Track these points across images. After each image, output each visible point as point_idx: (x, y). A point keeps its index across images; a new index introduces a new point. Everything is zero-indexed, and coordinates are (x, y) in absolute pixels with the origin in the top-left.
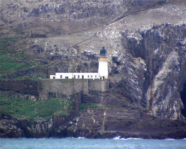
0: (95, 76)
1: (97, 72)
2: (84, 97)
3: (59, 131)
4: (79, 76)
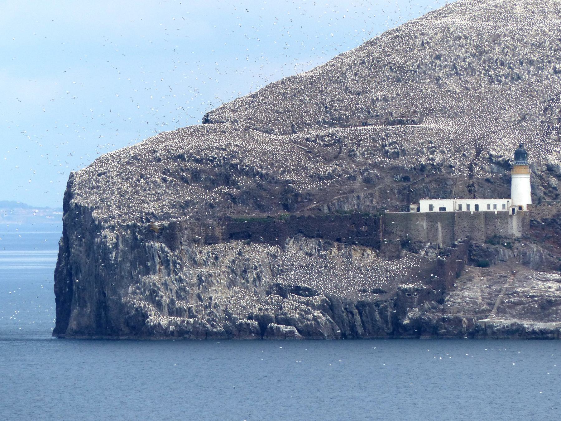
0: (501, 207)
1: (509, 196)
2: (475, 250)
3: (406, 322)
4: (468, 206)
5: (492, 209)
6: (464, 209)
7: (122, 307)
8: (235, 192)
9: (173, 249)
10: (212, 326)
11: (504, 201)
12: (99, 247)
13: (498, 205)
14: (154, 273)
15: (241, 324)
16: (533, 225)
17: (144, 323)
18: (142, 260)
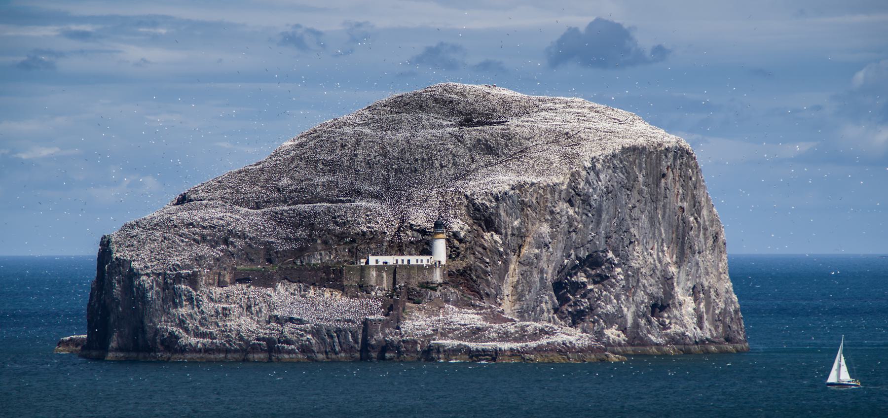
5: (419, 263)
6: (400, 263)
7: (157, 332)
8: (231, 248)
9: (196, 290)
10: (230, 345)
11: (428, 257)
12: (138, 289)
13: (425, 260)
14: (181, 307)
15: (254, 344)
16: (450, 274)
17: (176, 343)
18: (171, 297)
